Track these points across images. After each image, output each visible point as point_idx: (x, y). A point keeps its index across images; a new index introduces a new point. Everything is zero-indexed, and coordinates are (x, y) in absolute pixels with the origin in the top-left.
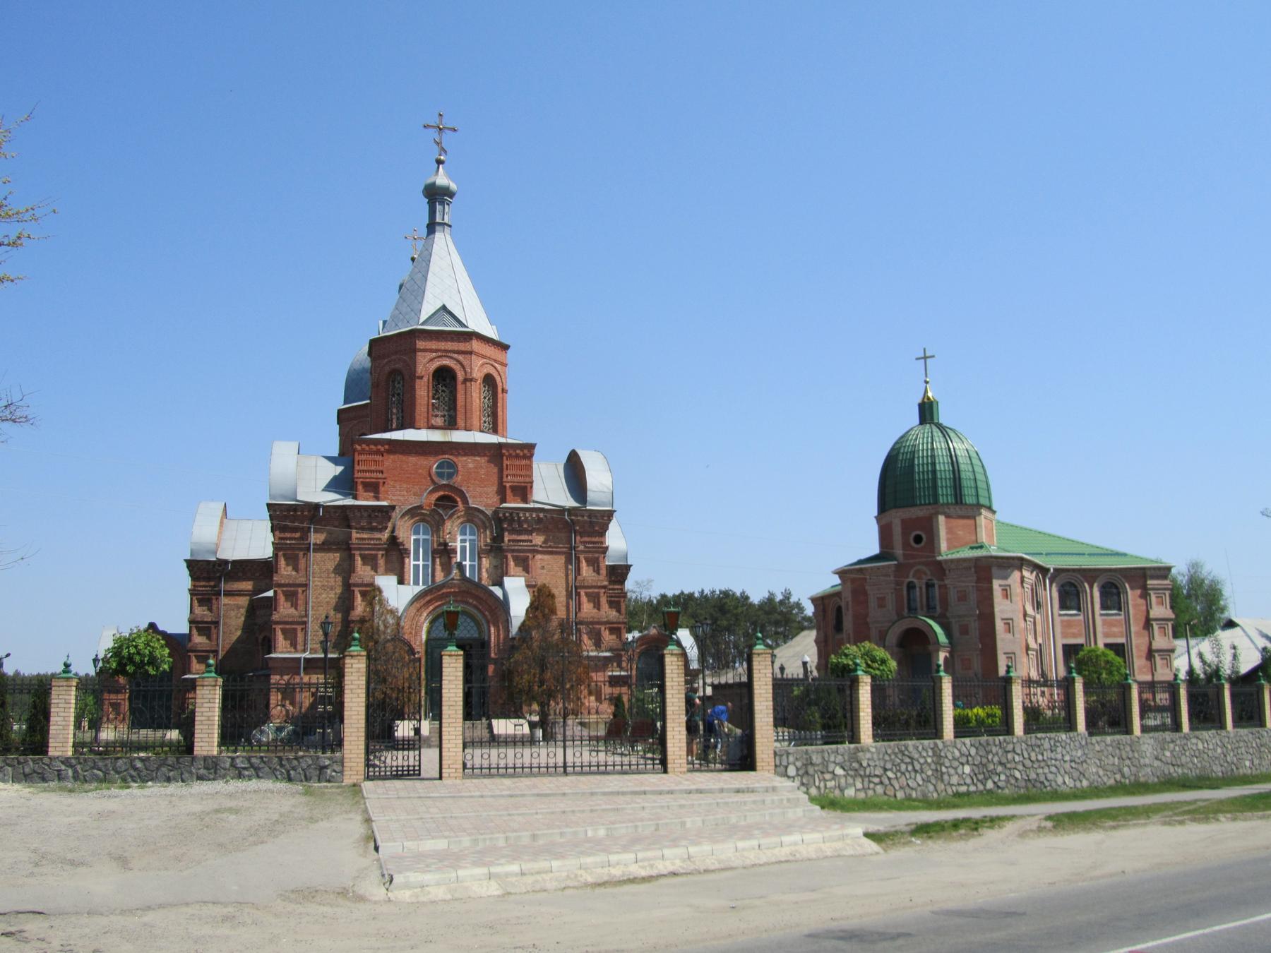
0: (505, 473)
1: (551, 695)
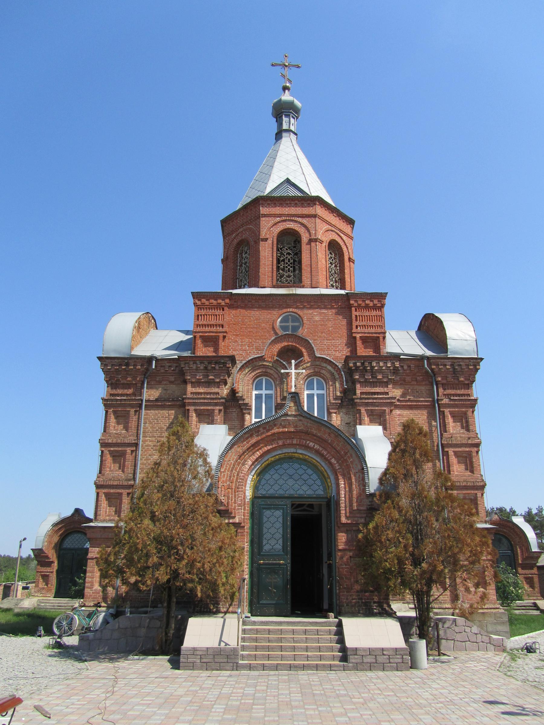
0: (354, 324)
1: (431, 579)
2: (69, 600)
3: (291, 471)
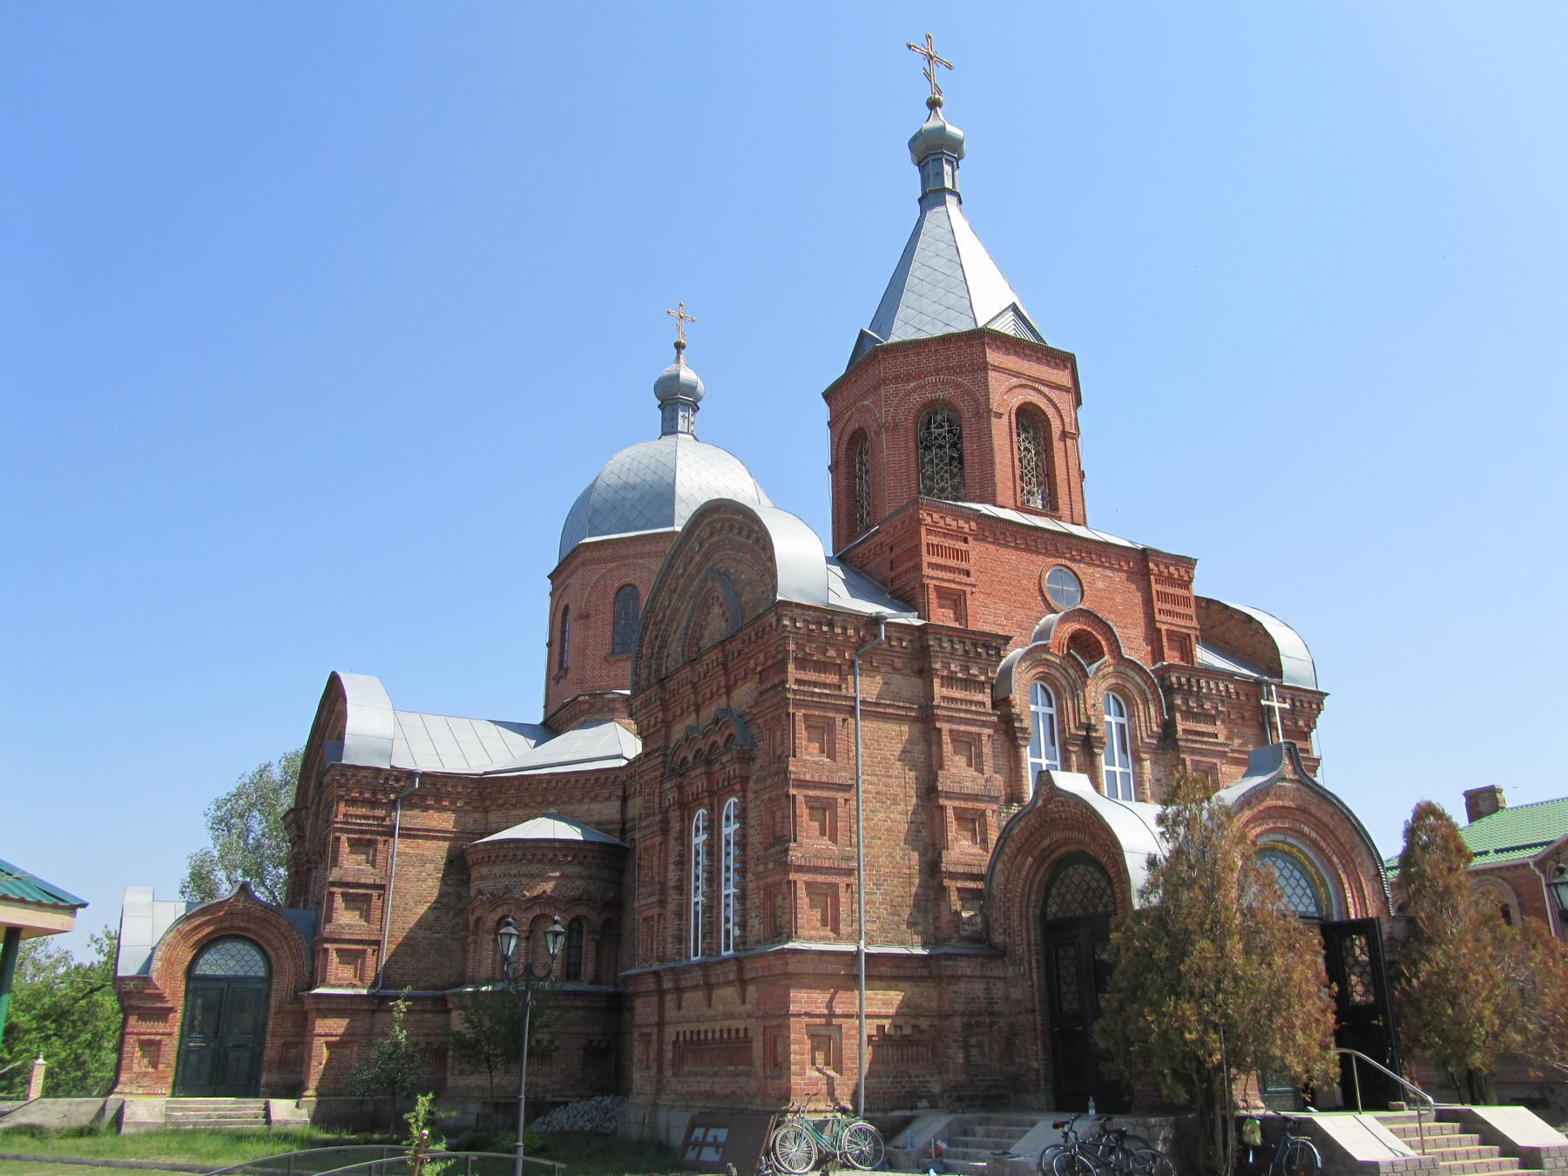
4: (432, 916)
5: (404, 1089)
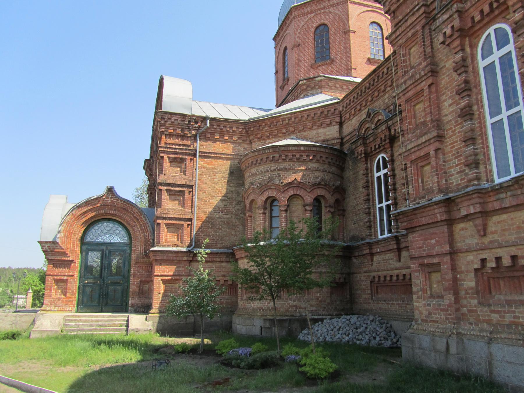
2: (110, 316)
3: (108, 228)
4: (222, 205)
5: (207, 311)
